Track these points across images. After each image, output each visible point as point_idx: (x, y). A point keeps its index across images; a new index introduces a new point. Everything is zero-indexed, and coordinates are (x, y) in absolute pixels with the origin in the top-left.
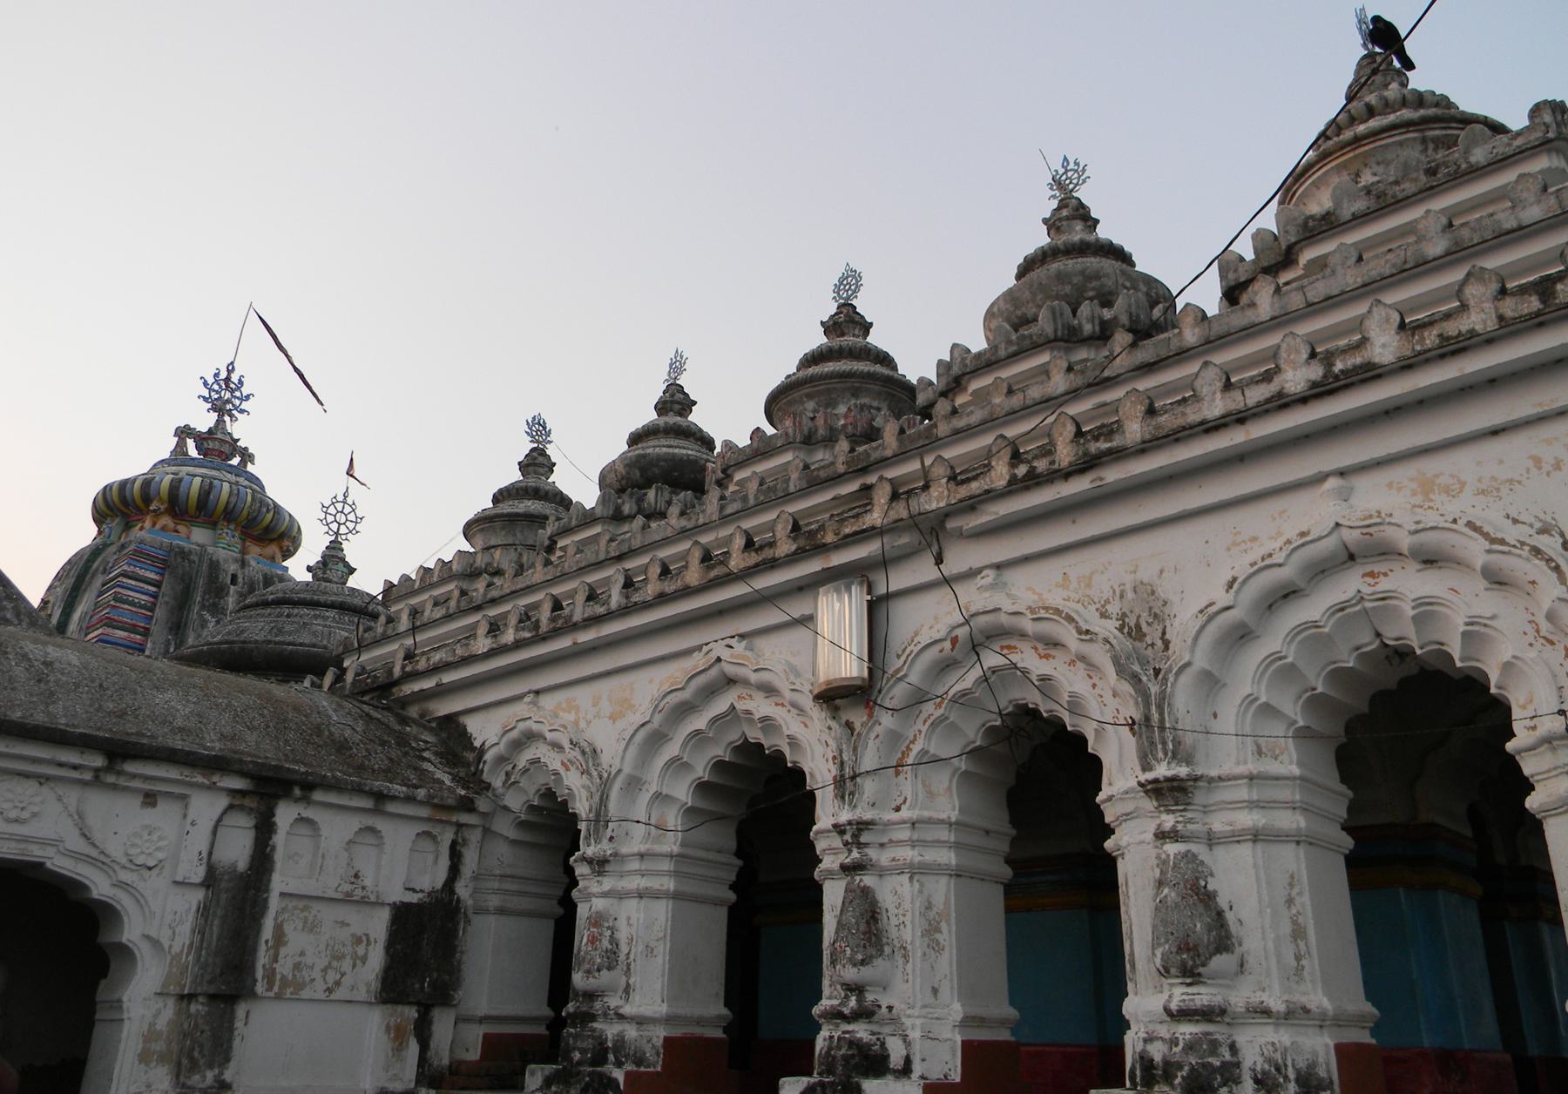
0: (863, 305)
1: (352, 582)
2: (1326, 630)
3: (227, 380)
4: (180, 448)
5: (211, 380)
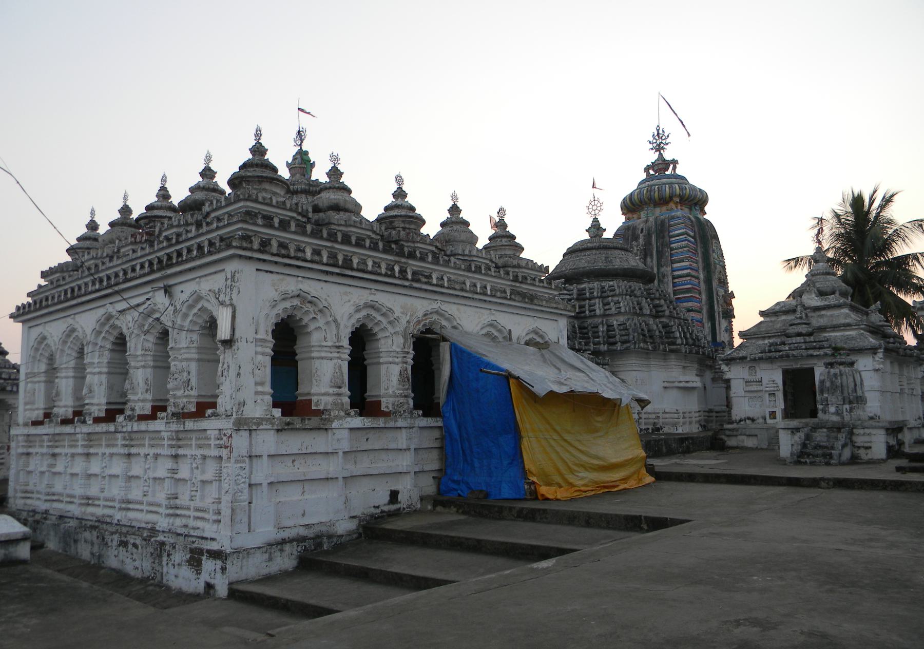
0: (213, 166)
1: (705, 217)
2: (909, 300)
3: (658, 134)
4: (648, 174)
5: (651, 139)
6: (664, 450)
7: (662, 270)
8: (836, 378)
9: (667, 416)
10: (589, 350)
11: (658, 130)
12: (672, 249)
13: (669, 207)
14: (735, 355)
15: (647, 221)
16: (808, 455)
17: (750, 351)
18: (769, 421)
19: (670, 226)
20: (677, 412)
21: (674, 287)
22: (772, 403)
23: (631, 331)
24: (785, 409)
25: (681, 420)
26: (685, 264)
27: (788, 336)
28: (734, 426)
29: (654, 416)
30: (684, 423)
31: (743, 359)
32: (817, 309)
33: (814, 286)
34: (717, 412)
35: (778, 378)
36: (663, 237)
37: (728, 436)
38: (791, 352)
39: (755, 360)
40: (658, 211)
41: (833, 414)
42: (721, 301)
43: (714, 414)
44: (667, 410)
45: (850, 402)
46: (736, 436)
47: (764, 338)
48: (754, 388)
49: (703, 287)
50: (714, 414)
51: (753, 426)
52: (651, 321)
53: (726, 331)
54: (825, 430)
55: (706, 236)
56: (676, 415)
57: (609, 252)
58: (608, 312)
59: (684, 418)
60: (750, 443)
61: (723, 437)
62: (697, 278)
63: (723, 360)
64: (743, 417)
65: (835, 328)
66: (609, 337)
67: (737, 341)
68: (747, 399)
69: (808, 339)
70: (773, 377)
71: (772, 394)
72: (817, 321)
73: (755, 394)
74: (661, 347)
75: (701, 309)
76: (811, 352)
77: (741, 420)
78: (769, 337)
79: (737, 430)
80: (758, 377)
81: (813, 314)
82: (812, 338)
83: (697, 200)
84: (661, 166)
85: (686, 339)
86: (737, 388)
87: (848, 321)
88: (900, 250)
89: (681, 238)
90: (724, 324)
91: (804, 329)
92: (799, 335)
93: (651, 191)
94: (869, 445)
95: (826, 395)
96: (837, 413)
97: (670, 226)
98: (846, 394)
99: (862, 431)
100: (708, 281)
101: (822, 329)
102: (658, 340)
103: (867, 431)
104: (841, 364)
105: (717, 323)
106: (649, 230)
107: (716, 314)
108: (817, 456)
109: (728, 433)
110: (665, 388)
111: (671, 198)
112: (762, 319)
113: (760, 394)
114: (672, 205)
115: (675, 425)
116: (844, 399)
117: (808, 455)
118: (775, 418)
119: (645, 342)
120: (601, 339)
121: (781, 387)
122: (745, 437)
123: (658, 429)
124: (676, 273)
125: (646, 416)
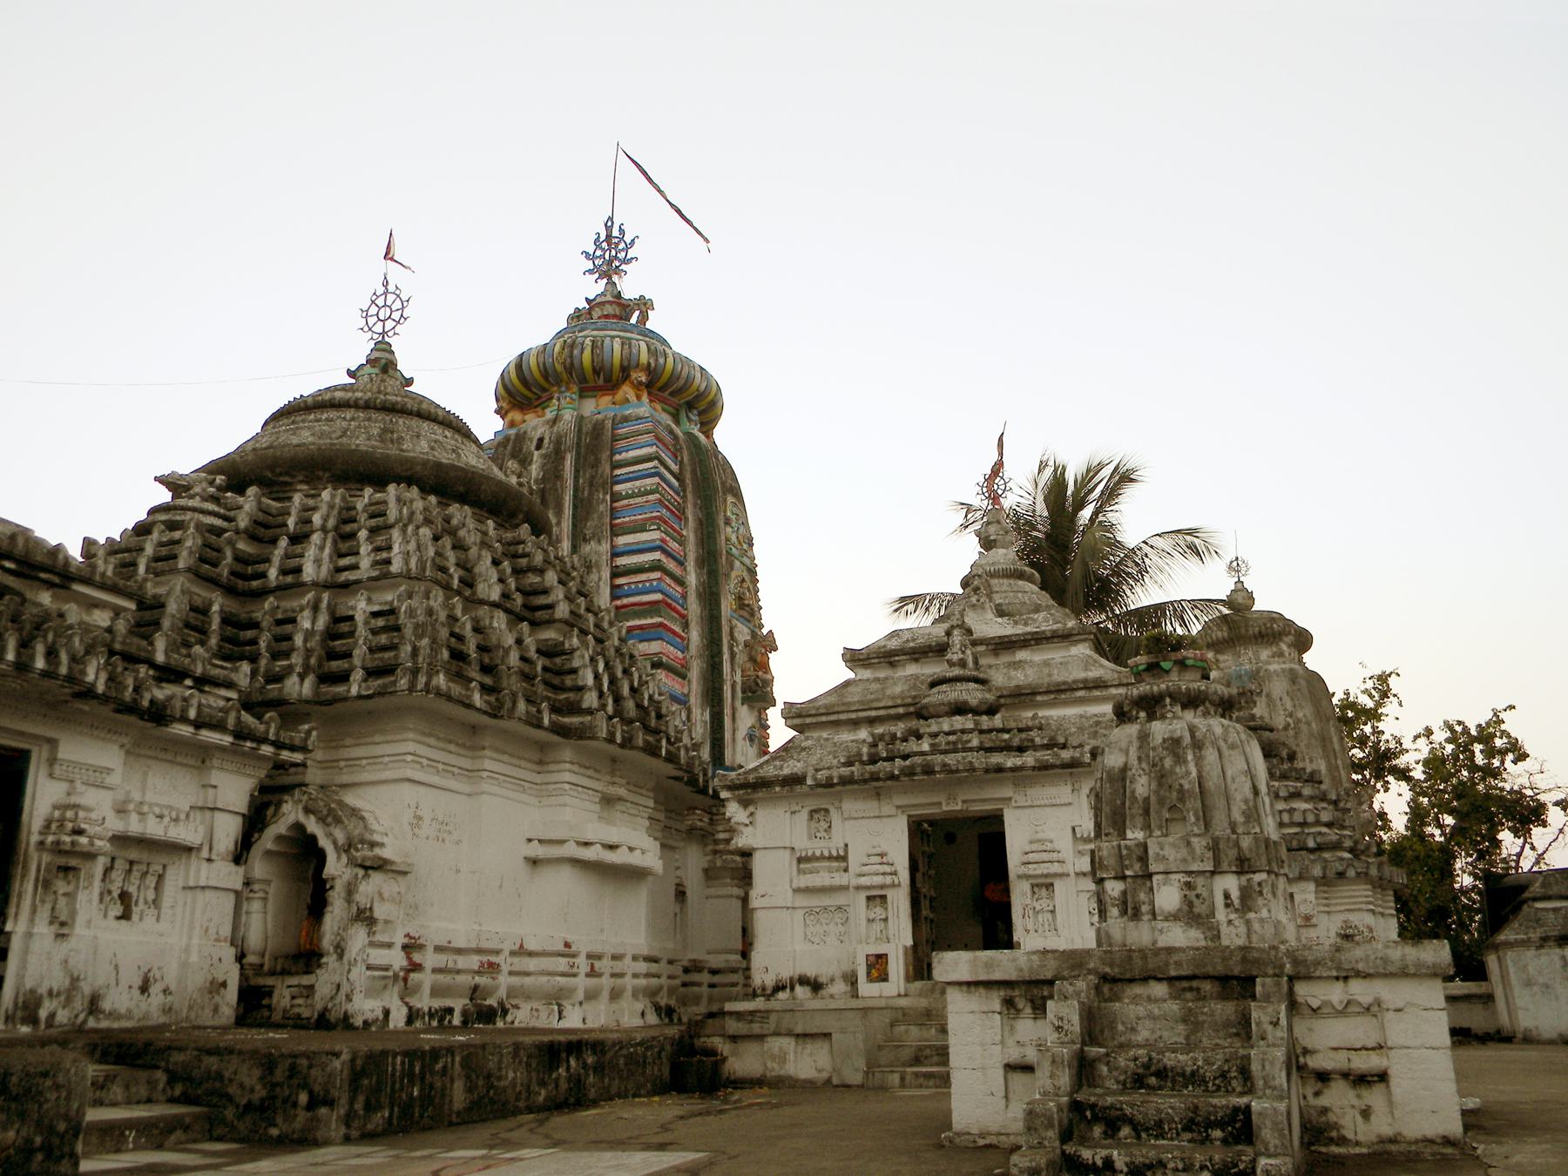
3: (609, 237)
6: (458, 1095)
7: (586, 549)
8: (1179, 759)
9: (532, 964)
10: (230, 685)
11: (609, 229)
12: (616, 497)
13: (620, 395)
14: (770, 771)
15: (555, 421)
16: (1112, 1122)
17: (813, 760)
18: (867, 989)
19: (615, 438)
20: (567, 951)
21: (614, 597)
22: (878, 926)
23: (408, 631)
24: (915, 946)
25: (581, 983)
26: (644, 535)
27: (922, 714)
28: (758, 1004)
29: (474, 961)
30: (591, 996)
31: (795, 780)
32: (1004, 645)
33: (991, 600)
34: (714, 972)
35: (894, 841)
36: (596, 464)
37: (734, 1039)
38: (939, 758)
39: (829, 784)
40: (589, 407)
41: (1174, 917)
42: (741, 658)
43: (705, 978)
44: (531, 945)
45: (1243, 866)
46: (761, 1037)
47: (855, 724)
48: (822, 878)
49: (694, 608)
50: (705, 978)
51: (817, 1004)
52: (499, 621)
53: (751, 738)
54: (1159, 989)
55: (709, 488)
56: (562, 964)
57: (401, 422)
58: (344, 577)
59: (592, 973)
60: (805, 1063)
61: (718, 1043)
62: (681, 582)
63: (731, 788)
64: (786, 974)
65: (1060, 692)
66: (332, 655)
67: (779, 734)
68: (799, 914)
69: (985, 722)
70: (879, 839)
71: (877, 899)
72: (1004, 674)
73: (827, 901)
74: (522, 706)
75: (686, 666)
76: (996, 759)
77: (779, 988)
78: (872, 721)
79: (764, 1015)
80: (834, 845)
81: (991, 660)
82: (997, 721)
83: (690, 399)
84: (609, 309)
85: (618, 699)
86: (773, 879)
87: (1094, 673)
88: (1141, 597)
89: (642, 476)
90: (746, 718)
91: (972, 694)
92: (960, 709)
93: (572, 346)
94: (1372, 1062)
95: (1135, 835)
96: (1191, 914)
97: (615, 438)
98: (1220, 828)
99: (1335, 994)
100: (710, 597)
101: (1023, 696)
102: (513, 683)
103: (1361, 991)
104: (1192, 701)
105: (727, 711)
106: (558, 441)
107: (727, 689)
108: (1158, 1129)
109: (733, 1026)
110: (534, 862)
111: (625, 370)
112: (850, 675)
113: (840, 899)
114: (627, 391)
115: (557, 999)
116: (1215, 847)
117: (1112, 1122)
118: (884, 978)
119: (459, 677)
120: (296, 659)
121: (904, 876)
122: (787, 1043)
123: (488, 1015)
124: (622, 561)
125: (441, 960)
